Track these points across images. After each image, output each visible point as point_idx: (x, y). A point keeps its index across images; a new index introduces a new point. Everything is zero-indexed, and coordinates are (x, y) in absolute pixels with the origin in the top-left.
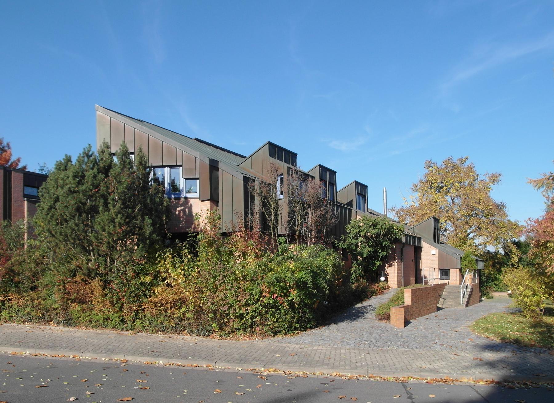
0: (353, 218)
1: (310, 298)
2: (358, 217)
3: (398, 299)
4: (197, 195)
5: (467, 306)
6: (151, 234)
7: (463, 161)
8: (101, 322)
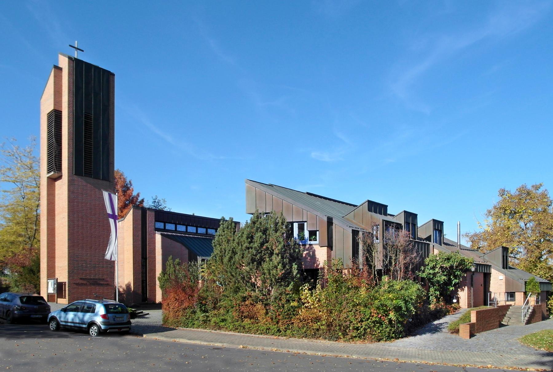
0: (431, 254)
1: (402, 317)
2: (436, 251)
3: (467, 317)
4: (317, 242)
5: (529, 322)
6: (296, 275)
7: (537, 188)
8: (265, 330)
